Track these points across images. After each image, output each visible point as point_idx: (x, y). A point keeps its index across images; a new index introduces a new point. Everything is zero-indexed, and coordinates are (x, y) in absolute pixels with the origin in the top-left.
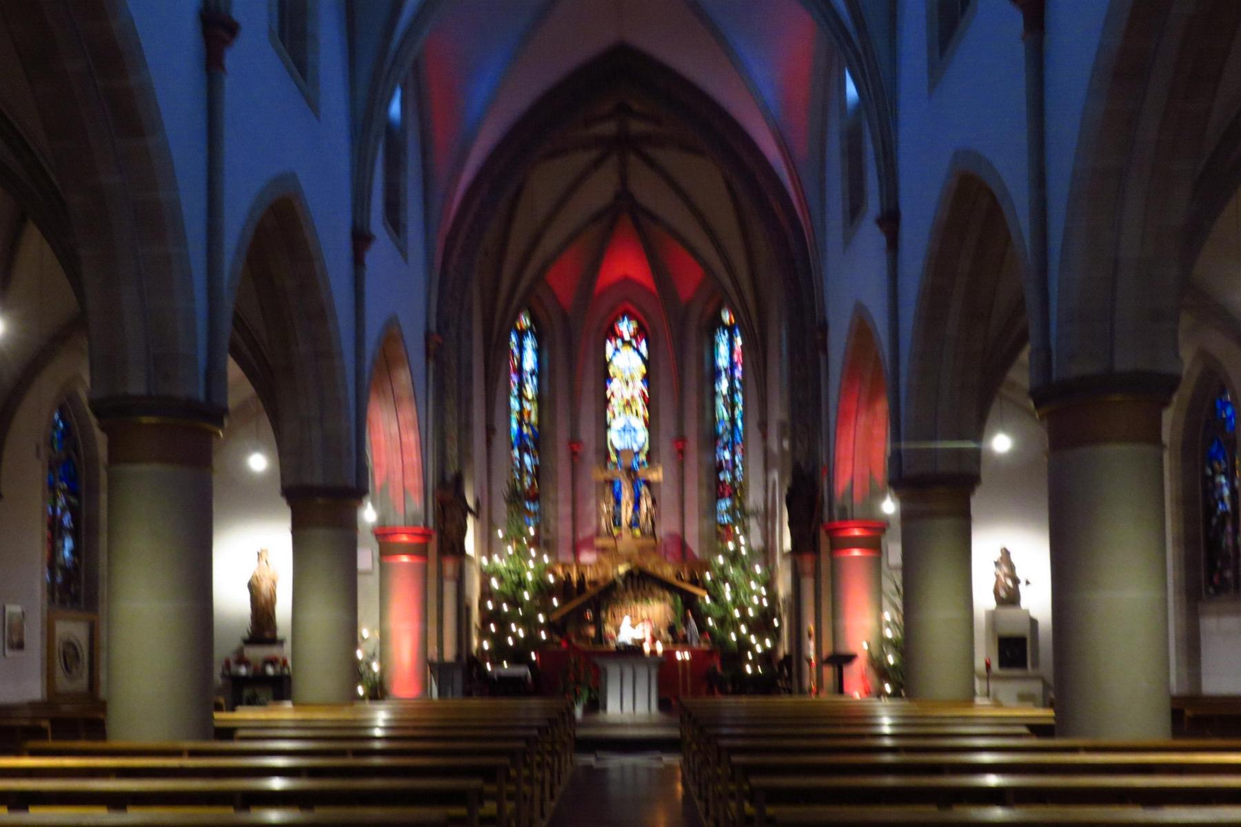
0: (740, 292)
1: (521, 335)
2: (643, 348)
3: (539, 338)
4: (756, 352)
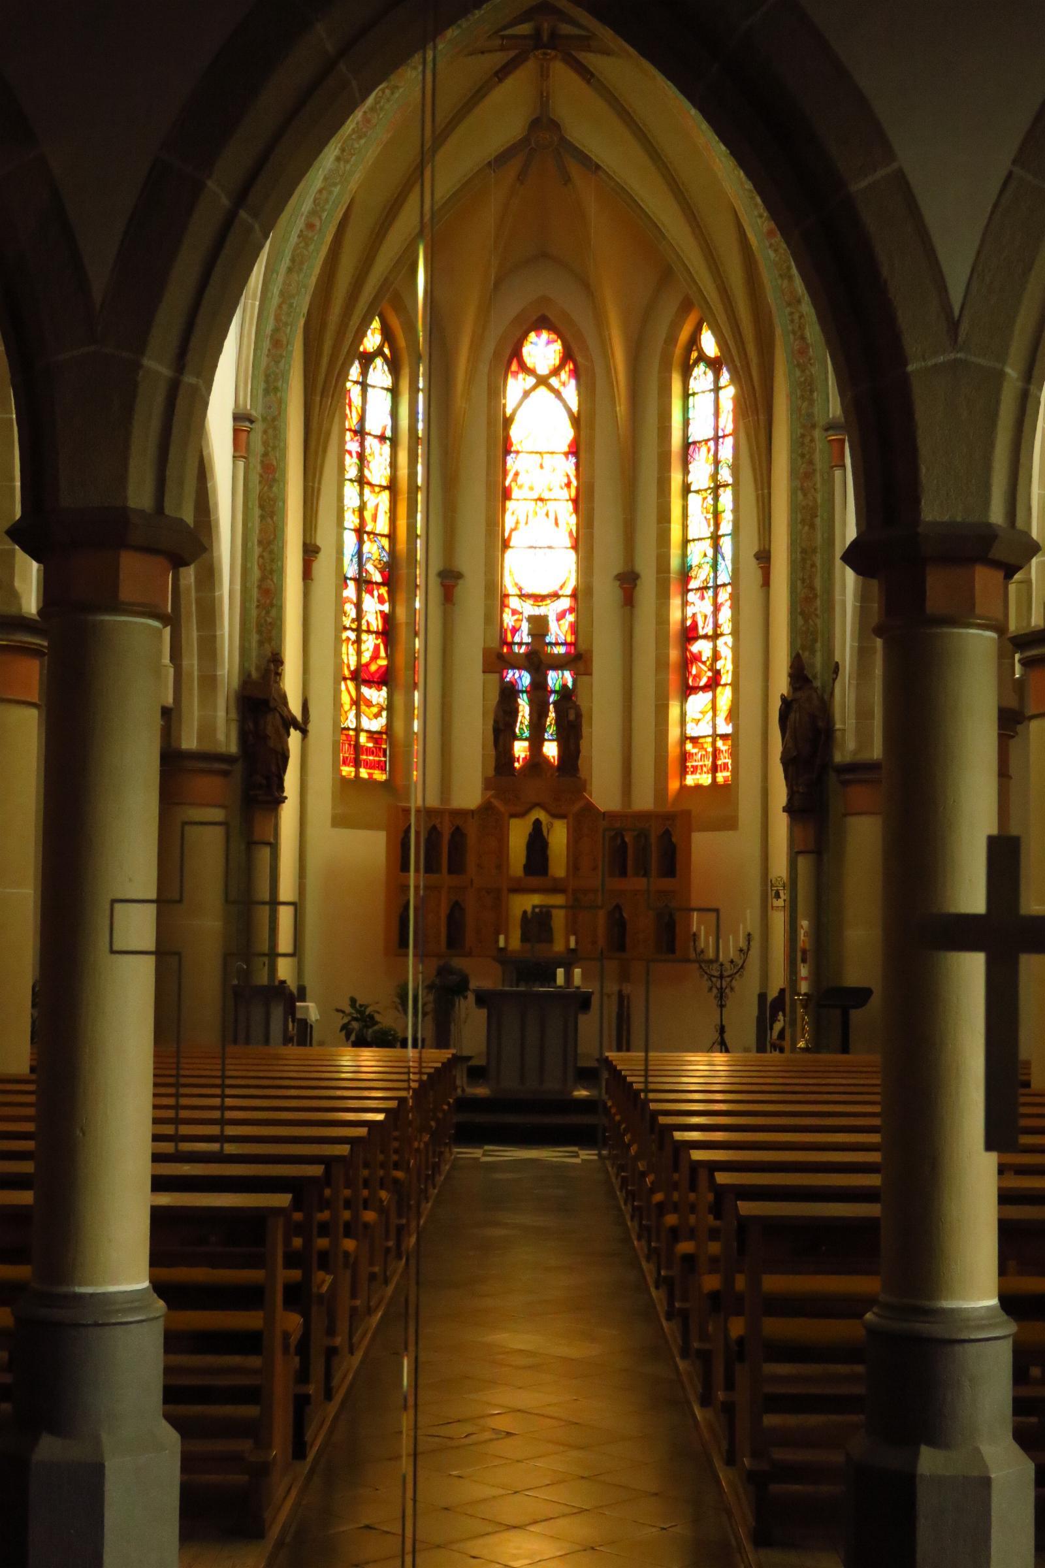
0: (724, 292)
1: (367, 360)
2: (571, 393)
3: (394, 367)
4: (755, 410)
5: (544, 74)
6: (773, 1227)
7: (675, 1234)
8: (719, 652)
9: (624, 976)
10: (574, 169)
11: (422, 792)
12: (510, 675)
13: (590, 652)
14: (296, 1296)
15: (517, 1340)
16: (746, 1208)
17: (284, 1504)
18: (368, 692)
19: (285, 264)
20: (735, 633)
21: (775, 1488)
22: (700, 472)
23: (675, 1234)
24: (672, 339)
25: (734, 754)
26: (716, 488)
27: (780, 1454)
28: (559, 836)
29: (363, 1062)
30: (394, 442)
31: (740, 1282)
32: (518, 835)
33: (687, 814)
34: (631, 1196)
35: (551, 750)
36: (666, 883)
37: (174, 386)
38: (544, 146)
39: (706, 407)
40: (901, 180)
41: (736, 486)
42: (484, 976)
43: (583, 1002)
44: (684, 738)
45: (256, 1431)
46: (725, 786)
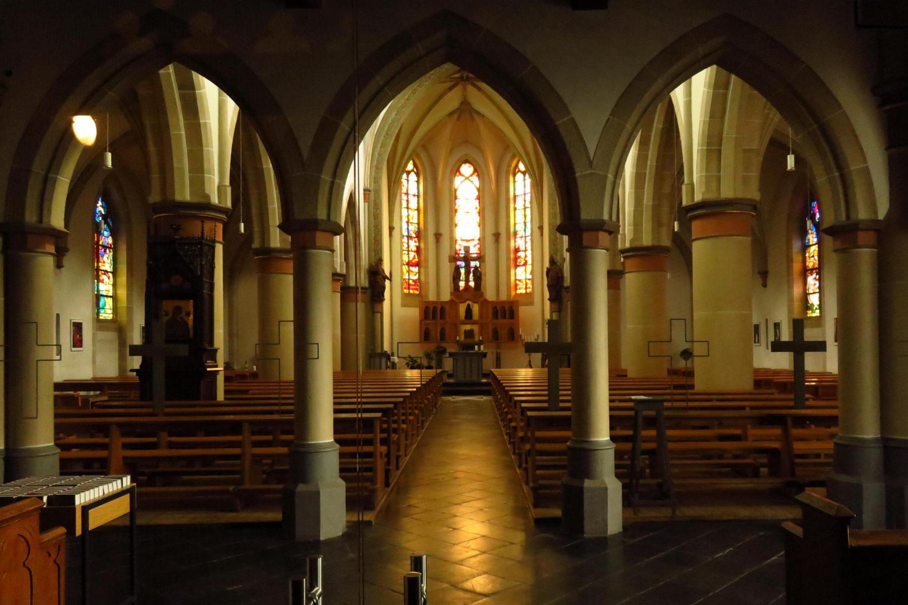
0: (527, 154)
1: (408, 173)
3: (418, 174)
4: (537, 186)
5: (465, 89)
6: (538, 419)
7: (511, 420)
8: (526, 255)
9: (498, 347)
10: (475, 116)
11: (432, 297)
12: (459, 263)
13: (484, 256)
14: (384, 442)
15: (463, 451)
16: (529, 413)
17: (381, 500)
18: (412, 268)
19: (379, 145)
20: (532, 249)
21: (540, 491)
22: (520, 204)
23: (511, 420)
24: (509, 166)
25: (533, 284)
26: (525, 208)
27: (541, 482)
28: (476, 308)
29: (412, 374)
30: (418, 196)
31: (529, 434)
32: (462, 308)
33: (517, 301)
34: (499, 409)
35: (472, 284)
36: (511, 321)
37: (332, 183)
38: (465, 110)
39: (521, 186)
40: (573, 121)
41: (531, 207)
42: (452, 348)
43: (485, 355)
44: (516, 280)
45: (372, 480)
46: (530, 294)
